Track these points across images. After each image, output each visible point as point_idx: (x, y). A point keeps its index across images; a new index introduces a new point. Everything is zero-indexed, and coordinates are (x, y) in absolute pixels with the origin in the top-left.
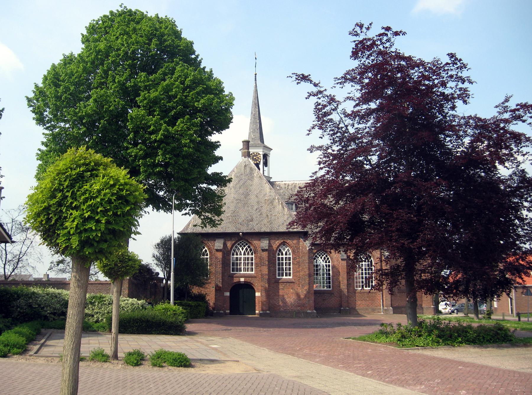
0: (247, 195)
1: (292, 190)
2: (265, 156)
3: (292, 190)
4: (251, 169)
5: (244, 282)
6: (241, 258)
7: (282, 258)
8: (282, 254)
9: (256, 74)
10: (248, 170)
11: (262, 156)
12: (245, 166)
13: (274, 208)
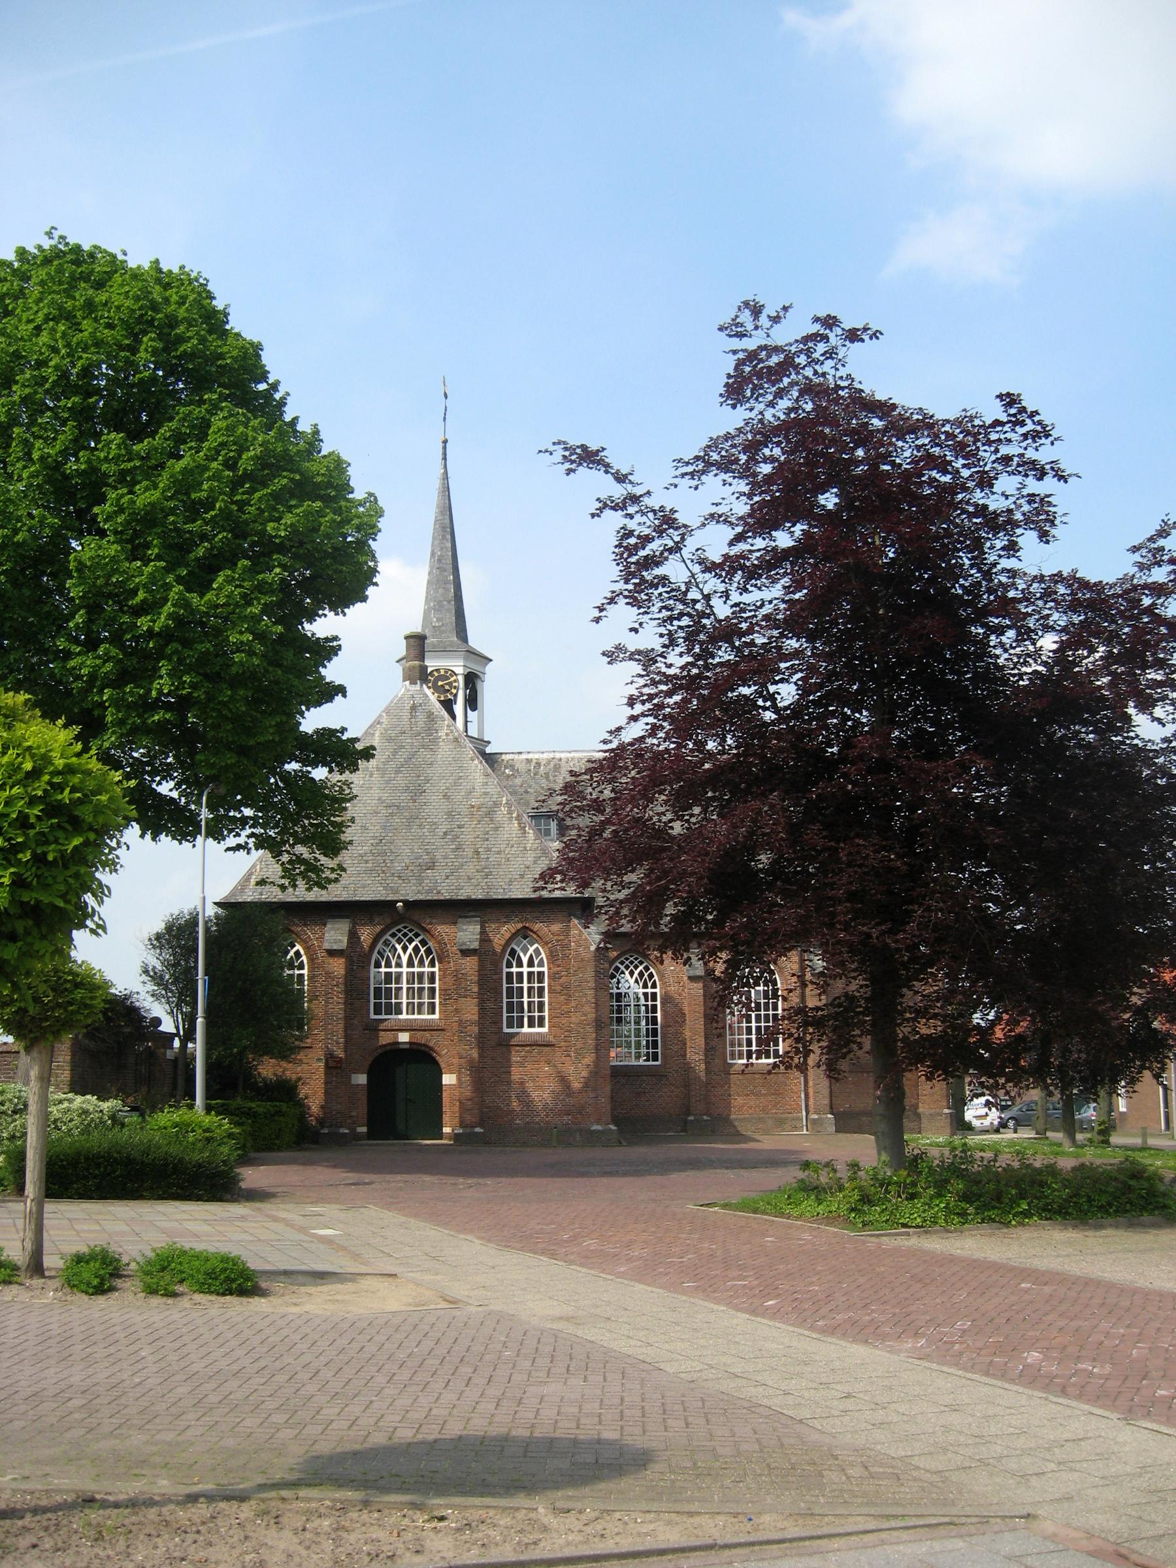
0: (417, 792)
1: (547, 778)
2: (472, 680)
3: (547, 778)
4: (430, 716)
5: (410, 1043)
6: (399, 975)
7: (520, 975)
10: (421, 717)
11: (461, 679)
12: (414, 708)
13: (496, 829)
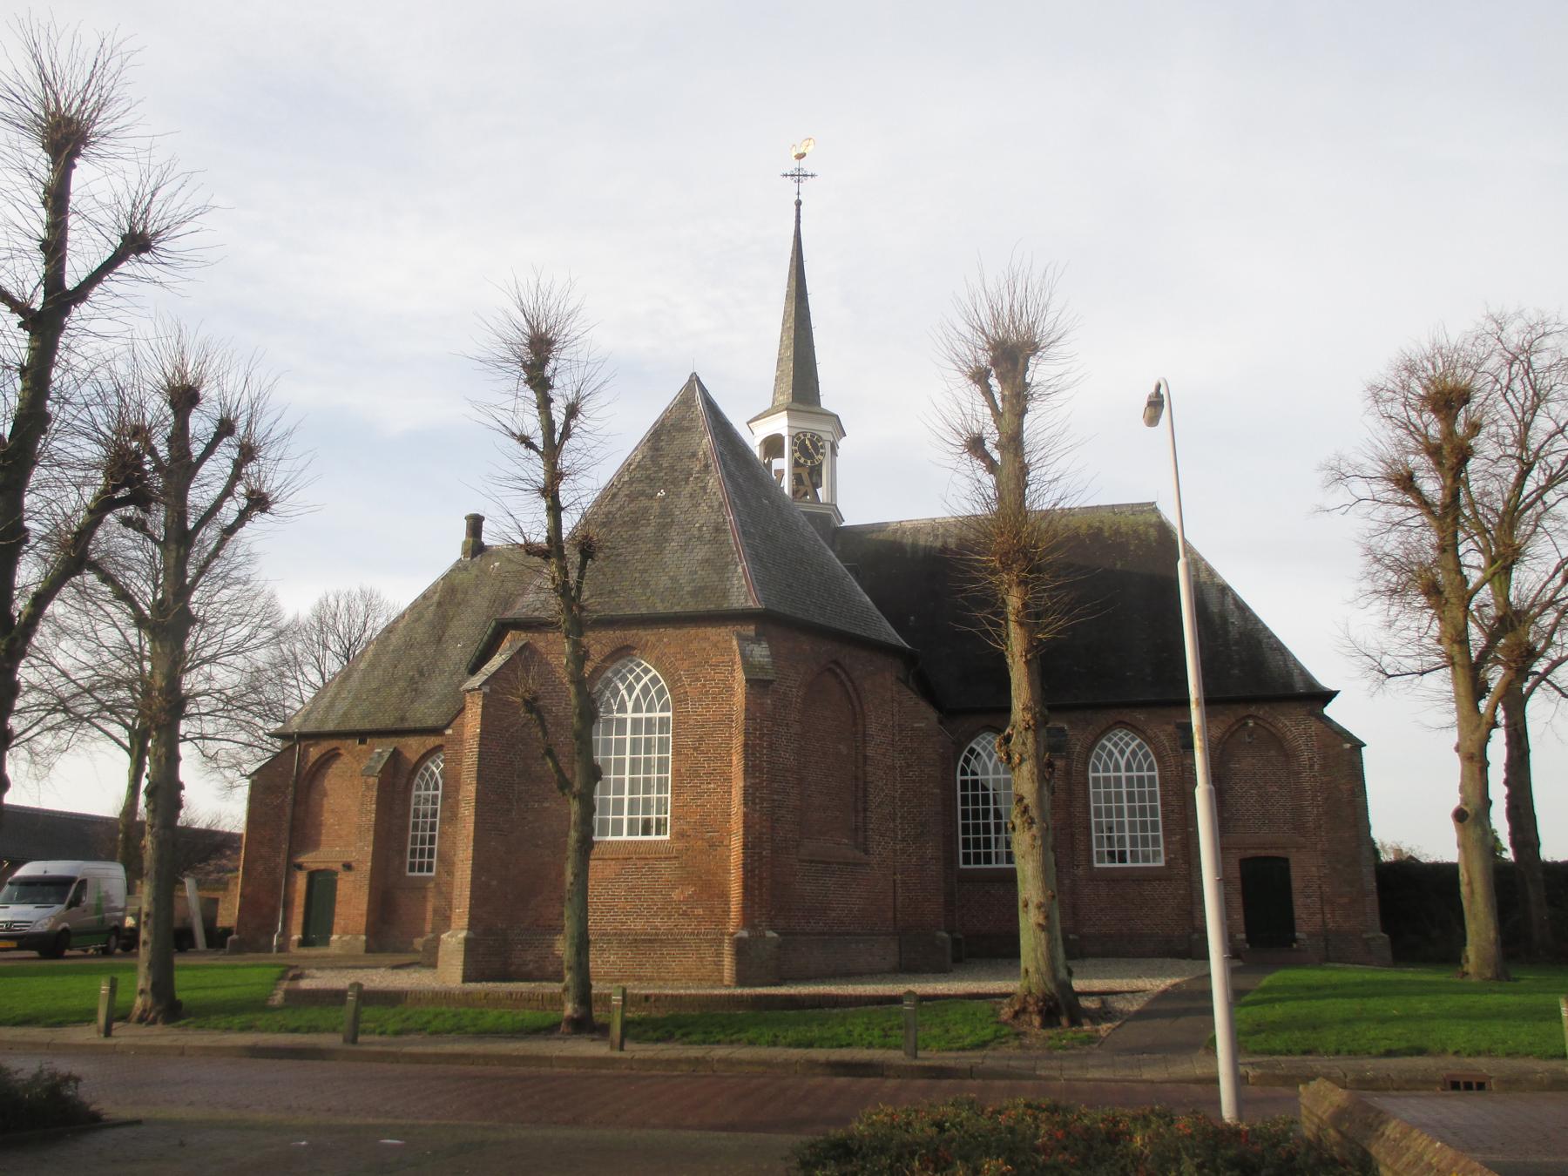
7: (1118, 780)
8: (1117, 768)
9: (799, 203)
